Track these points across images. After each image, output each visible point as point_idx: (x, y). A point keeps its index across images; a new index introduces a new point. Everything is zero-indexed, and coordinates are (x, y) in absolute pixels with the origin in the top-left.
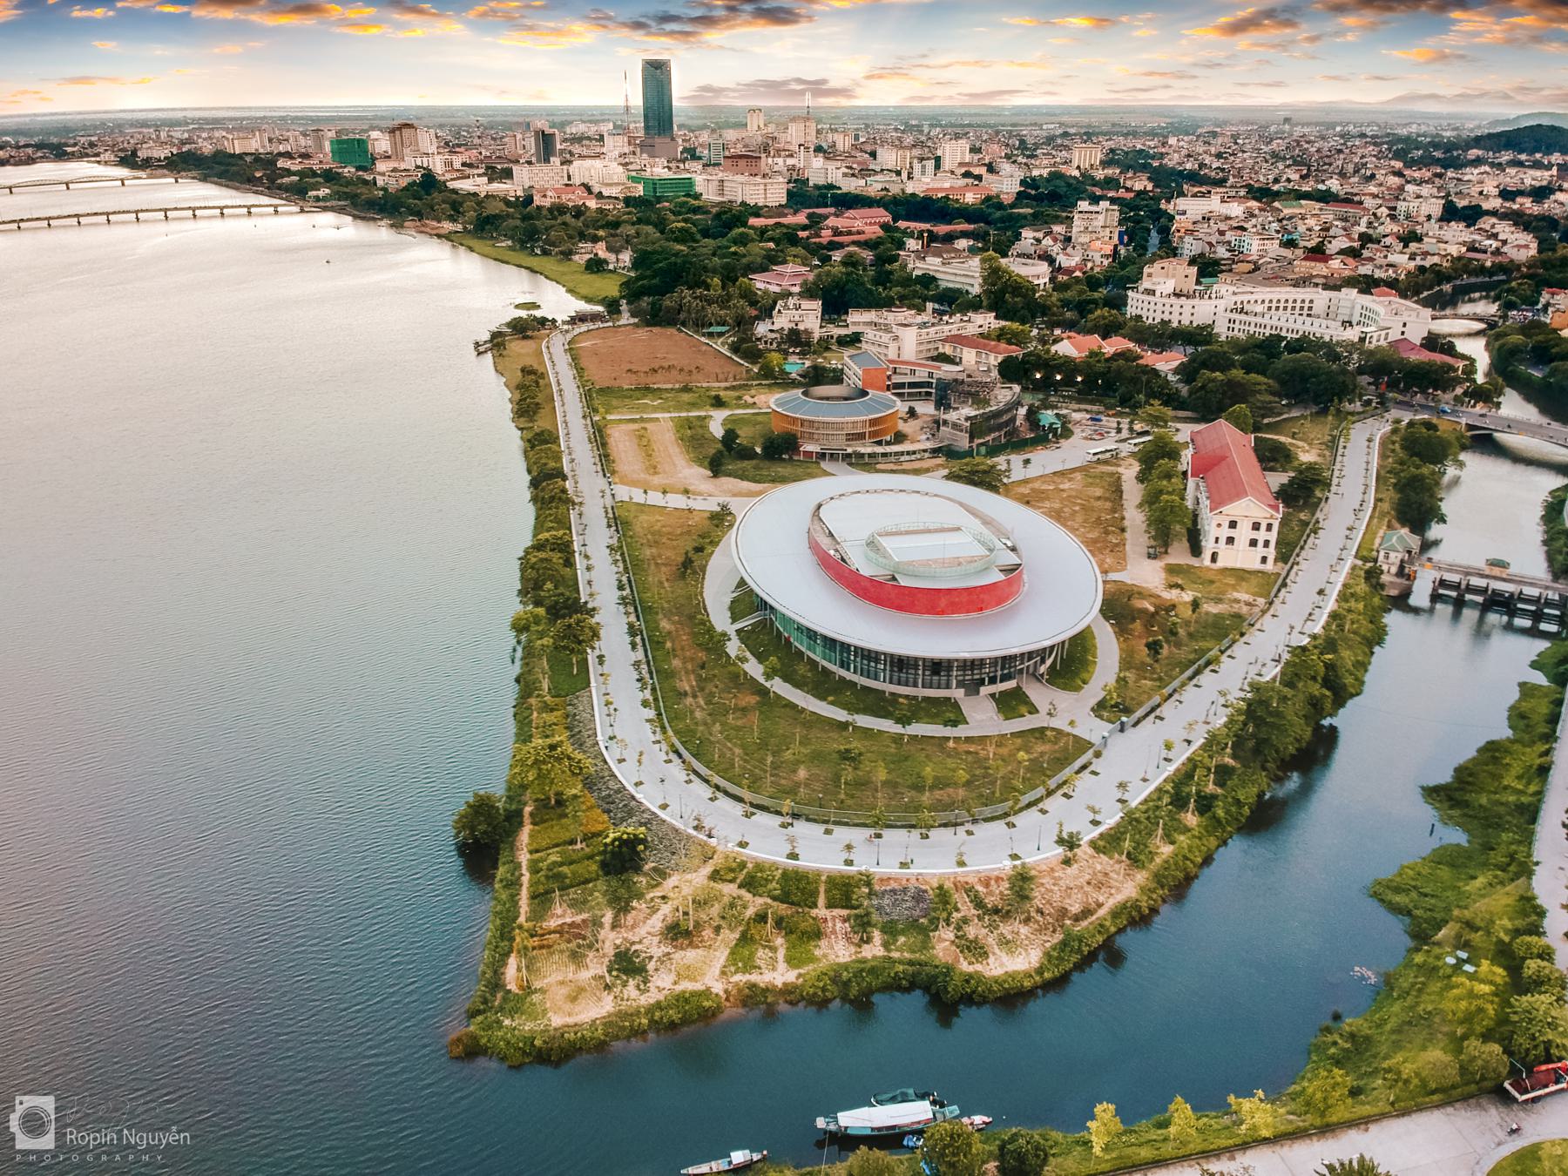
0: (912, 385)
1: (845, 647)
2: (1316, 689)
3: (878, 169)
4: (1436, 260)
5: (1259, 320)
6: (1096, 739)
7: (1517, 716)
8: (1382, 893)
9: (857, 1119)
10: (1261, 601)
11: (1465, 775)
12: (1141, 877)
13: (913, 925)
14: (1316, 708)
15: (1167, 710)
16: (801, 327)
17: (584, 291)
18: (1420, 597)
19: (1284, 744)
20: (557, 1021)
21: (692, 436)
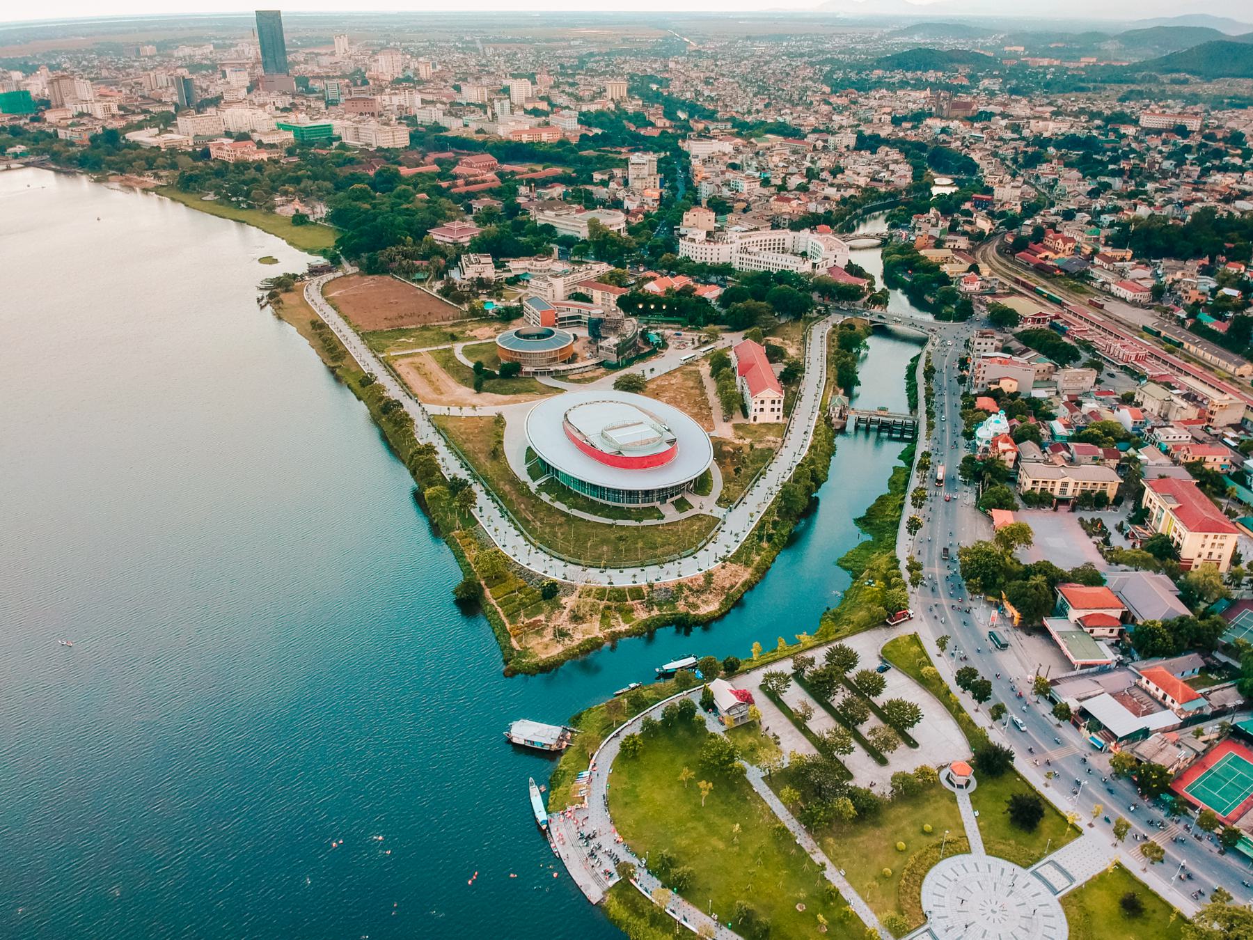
0: (569, 318)
1: (603, 488)
2: (809, 483)
3: (464, 102)
4: (851, 192)
5: (756, 258)
6: (721, 517)
7: (892, 483)
8: (842, 563)
9: (670, 666)
10: (779, 440)
11: (871, 512)
12: (750, 570)
13: (667, 601)
14: (809, 491)
15: (748, 499)
16: (484, 276)
17: (303, 244)
18: (850, 427)
19: (797, 510)
20: (544, 657)
21: (449, 364)
